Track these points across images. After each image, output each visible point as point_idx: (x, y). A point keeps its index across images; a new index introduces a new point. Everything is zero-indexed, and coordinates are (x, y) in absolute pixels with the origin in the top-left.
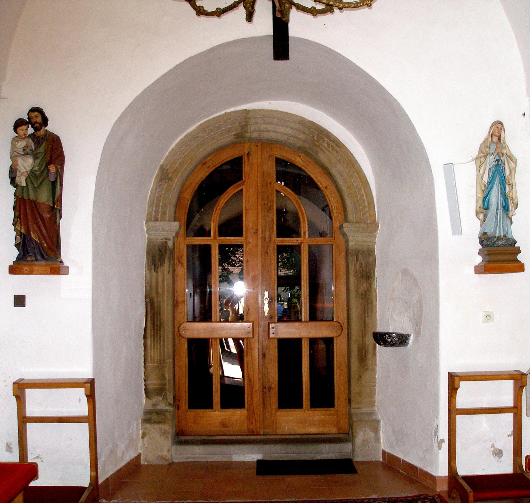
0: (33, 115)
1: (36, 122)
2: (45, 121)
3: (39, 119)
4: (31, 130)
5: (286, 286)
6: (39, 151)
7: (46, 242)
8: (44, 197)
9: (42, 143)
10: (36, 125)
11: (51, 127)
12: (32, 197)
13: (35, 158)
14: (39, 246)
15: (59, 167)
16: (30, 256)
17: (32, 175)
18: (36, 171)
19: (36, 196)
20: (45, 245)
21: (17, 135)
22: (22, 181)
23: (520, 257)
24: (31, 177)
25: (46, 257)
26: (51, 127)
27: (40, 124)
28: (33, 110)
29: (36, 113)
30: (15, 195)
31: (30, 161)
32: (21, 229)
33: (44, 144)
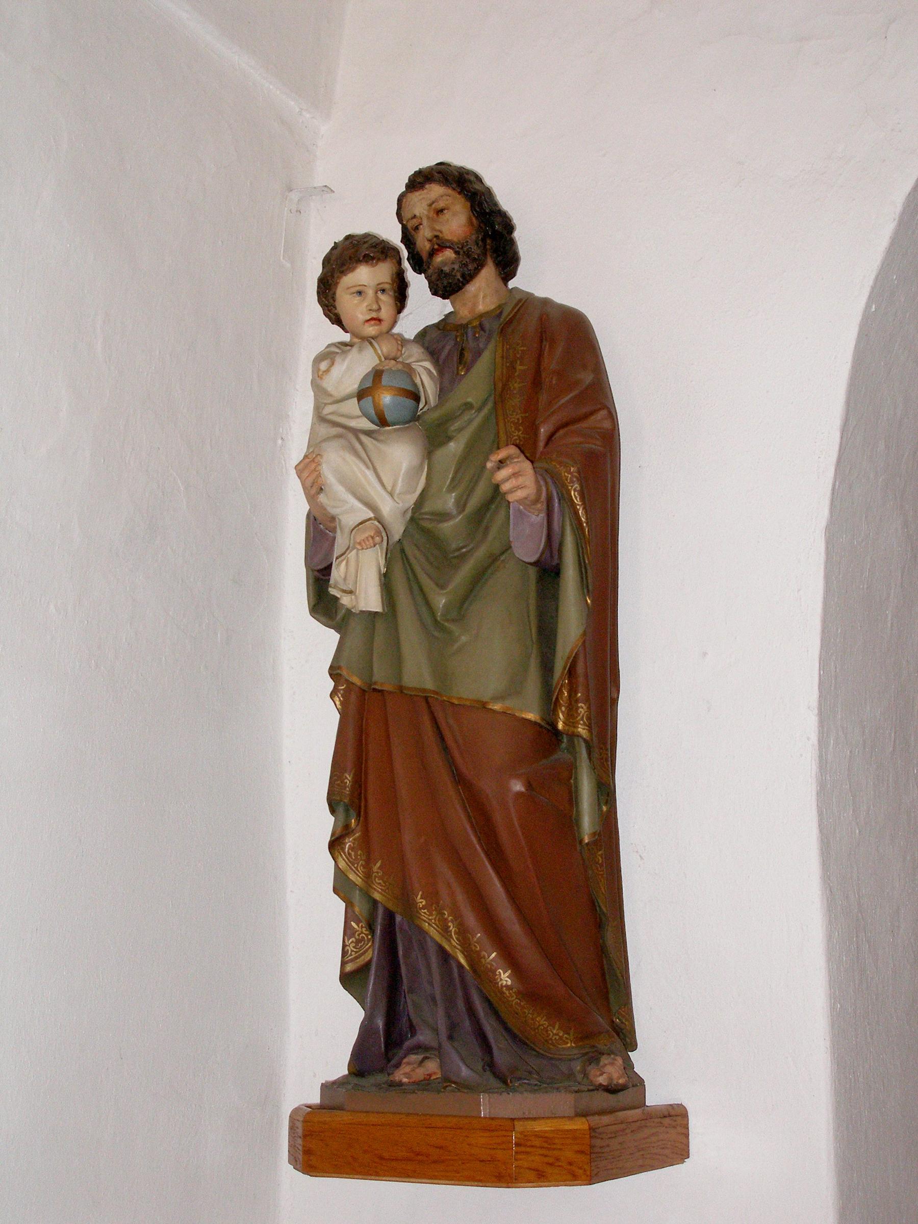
0: (419, 204)
1: (440, 244)
2: (494, 237)
3: (457, 223)
4: (425, 308)
5: (417, 922)
6: (453, 403)
7: (511, 959)
8: (489, 668)
9: (478, 354)
10: (439, 259)
11: (538, 277)
12: (417, 673)
13: (434, 437)
14: (465, 988)
15: (570, 474)
16: (417, 1048)
17: (417, 550)
18: (443, 516)
19: (441, 672)
20: (505, 978)
21: (346, 337)
22: (362, 582)
23: (655, 1097)
24: (410, 550)
25: (503, 1054)
26: (541, 275)
27: (460, 249)
28: (419, 180)
29: (435, 191)
30: (335, 672)
31: (401, 455)
32: (368, 876)
33: (486, 356)
